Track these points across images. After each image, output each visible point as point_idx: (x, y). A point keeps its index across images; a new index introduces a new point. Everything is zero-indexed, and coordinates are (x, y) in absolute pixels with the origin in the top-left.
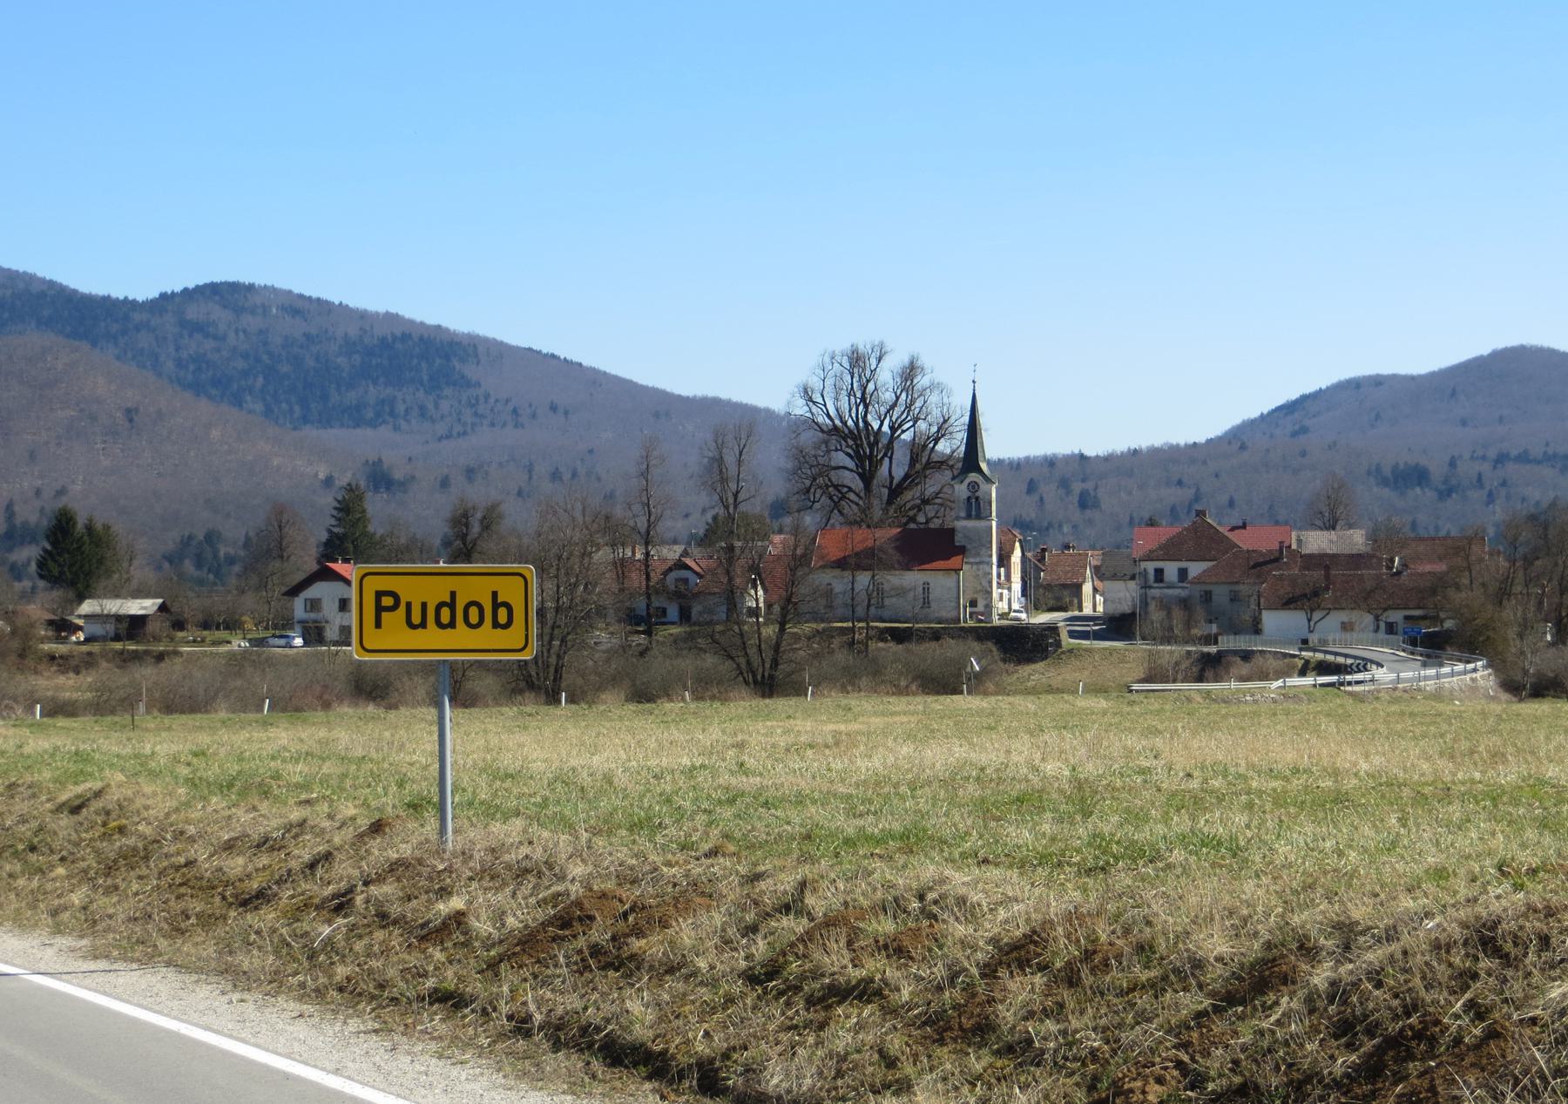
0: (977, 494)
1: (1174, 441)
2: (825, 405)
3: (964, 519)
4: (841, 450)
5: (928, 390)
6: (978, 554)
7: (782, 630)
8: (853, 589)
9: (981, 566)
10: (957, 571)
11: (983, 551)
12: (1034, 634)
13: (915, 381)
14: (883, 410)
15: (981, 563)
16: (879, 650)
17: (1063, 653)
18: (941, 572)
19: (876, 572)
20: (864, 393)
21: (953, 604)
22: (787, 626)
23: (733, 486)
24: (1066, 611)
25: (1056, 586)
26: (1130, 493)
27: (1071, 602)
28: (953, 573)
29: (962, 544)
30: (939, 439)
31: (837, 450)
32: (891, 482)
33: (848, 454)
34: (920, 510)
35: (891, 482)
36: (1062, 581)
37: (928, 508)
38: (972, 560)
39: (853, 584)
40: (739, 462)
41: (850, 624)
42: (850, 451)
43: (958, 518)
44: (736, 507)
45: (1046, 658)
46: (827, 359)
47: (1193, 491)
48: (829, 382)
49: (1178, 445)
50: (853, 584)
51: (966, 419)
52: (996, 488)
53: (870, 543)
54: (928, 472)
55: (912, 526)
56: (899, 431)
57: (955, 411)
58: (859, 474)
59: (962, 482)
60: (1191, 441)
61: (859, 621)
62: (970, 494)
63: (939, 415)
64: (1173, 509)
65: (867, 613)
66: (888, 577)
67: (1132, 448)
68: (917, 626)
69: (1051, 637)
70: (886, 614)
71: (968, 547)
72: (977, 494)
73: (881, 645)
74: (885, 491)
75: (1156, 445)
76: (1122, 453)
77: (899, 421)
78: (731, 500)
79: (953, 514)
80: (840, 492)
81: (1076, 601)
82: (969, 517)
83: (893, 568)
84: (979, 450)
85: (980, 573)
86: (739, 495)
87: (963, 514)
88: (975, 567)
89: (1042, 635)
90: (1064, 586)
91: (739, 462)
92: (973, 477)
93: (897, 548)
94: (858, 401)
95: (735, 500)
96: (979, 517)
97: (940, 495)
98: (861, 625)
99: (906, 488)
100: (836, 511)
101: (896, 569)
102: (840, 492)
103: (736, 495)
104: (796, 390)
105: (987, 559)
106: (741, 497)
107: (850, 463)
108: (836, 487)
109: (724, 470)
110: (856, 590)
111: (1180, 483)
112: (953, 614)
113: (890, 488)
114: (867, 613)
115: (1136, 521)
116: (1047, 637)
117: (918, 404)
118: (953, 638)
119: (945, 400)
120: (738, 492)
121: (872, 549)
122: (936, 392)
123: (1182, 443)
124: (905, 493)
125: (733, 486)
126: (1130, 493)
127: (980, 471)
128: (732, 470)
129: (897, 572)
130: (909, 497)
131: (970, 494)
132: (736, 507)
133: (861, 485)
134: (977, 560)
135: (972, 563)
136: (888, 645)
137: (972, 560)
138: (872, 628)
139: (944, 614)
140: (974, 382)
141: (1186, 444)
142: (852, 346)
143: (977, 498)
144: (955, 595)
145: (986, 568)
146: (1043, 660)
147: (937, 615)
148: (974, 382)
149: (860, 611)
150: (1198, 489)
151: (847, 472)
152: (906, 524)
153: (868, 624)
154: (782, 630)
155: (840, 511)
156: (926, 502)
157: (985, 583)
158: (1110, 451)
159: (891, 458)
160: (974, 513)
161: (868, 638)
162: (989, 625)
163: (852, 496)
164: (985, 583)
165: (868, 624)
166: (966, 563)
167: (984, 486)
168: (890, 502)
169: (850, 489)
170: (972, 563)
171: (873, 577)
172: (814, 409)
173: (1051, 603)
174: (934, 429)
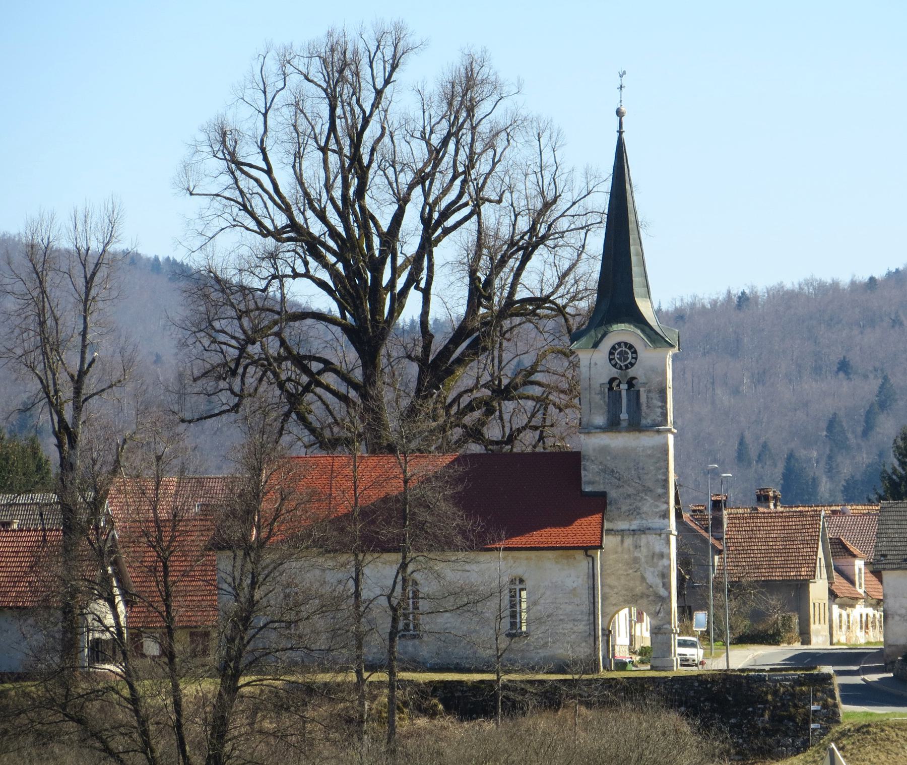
0: (632, 372)
1: (826, 277)
2: (269, 172)
3: (604, 429)
4: (307, 275)
5: (503, 135)
6: (635, 512)
7: (230, 688)
8: (357, 594)
9: (644, 540)
10: (588, 550)
11: (648, 505)
12: (775, 693)
13: (479, 113)
14: (406, 178)
15: (643, 531)
16: (417, 734)
17: (844, 734)
18: (550, 554)
19: (412, 554)
20: (356, 145)
21: (582, 627)
22: (242, 681)
23: (72, 360)
24: (777, 643)
25: (751, 585)
26: (736, 391)
27: (786, 621)
28: (580, 555)
29: (600, 488)
30: (535, 247)
31: (296, 275)
32: (427, 348)
33: (322, 284)
34: (490, 411)
35: (427, 348)
36: (764, 574)
37: (509, 406)
38: (622, 525)
39: (357, 581)
40: (86, 301)
41: (352, 677)
42: (325, 276)
43: (585, 428)
44: (78, 409)
45: (805, 746)
46: (272, 66)
47: (874, 384)
48: (280, 118)
49: (835, 286)
50: (357, 581)
51: (601, 201)
52: (675, 357)
53: (394, 488)
54: (506, 324)
55: (475, 448)
56: (439, 231)
57: (570, 182)
58: (346, 329)
59: (596, 345)
60: (863, 276)
61: (373, 668)
62: (615, 372)
63: (533, 191)
64: (832, 424)
65: (391, 651)
66: (439, 566)
67: (736, 291)
68: (505, 678)
69: (816, 699)
70: (426, 650)
71: (613, 494)
72: (632, 372)
73: (422, 722)
74: (413, 369)
75: (788, 286)
76: (714, 303)
77: (444, 203)
78: (67, 393)
79: (571, 416)
80: (306, 370)
81: (795, 620)
82: (613, 425)
83: (447, 544)
84: (635, 269)
85: (642, 554)
86: (86, 380)
87: (600, 420)
88: (629, 541)
89: (793, 695)
90: (769, 586)
91: (86, 301)
92: (620, 332)
93: (459, 500)
94: (347, 163)
95: (77, 391)
96: (636, 426)
97: (538, 377)
98: (376, 677)
99: (460, 361)
100: (294, 416)
101: (457, 549)
102: (306, 370)
103: (78, 381)
104: (202, 137)
105: (657, 522)
106: (91, 384)
107: (326, 304)
108: (300, 361)
109: (50, 322)
110: (365, 594)
111: (844, 367)
112: (583, 651)
113: (422, 362)
114: (391, 651)
115: (753, 452)
116: (807, 699)
117: (483, 166)
118: (589, 705)
119: (548, 156)
120: (82, 373)
121: (402, 500)
122: (519, 138)
123: (845, 280)
124: (459, 372)
125: (72, 360)
126: (736, 391)
127: (638, 319)
128: (70, 321)
129: (461, 555)
130: (470, 383)
131: (615, 372)
132: (78, 409)
133: (352, 355)
134: (635, 525)
135: (622, 533)
136: (439, 722)
137: (622, 525)
138: (405, 683)
139: (564, 651)
140: (619, 113)
141: (853, 283)
142: (330, 34)
143: (631, 383)
144: (585, 607)
145: (657, 545)
146: (797, 752)
147: (543, 653)
148: (619, 113)
149: (375, 646)
150: (886, 379)
151: (321, 326)
152: (460, 443)
153: (392, 674)
154: (230, 688)
155: (302, 419)
156: (504, 393)
157: (652, 578)
158: (688, 300)
159: (426, 293)
160: (624, 416)
161: (393, 707)
162: (663, 674)
163: (330, 379)
164: (652, 578)
165: (392, 674)
166: (609, 531)
167: (647, 354)
168: (423, 392)
169: (328, 366)
170: (622, 533)
171: (404, 566)
172: (244, 182)
173: (744, 625)
174: (523, 224)
